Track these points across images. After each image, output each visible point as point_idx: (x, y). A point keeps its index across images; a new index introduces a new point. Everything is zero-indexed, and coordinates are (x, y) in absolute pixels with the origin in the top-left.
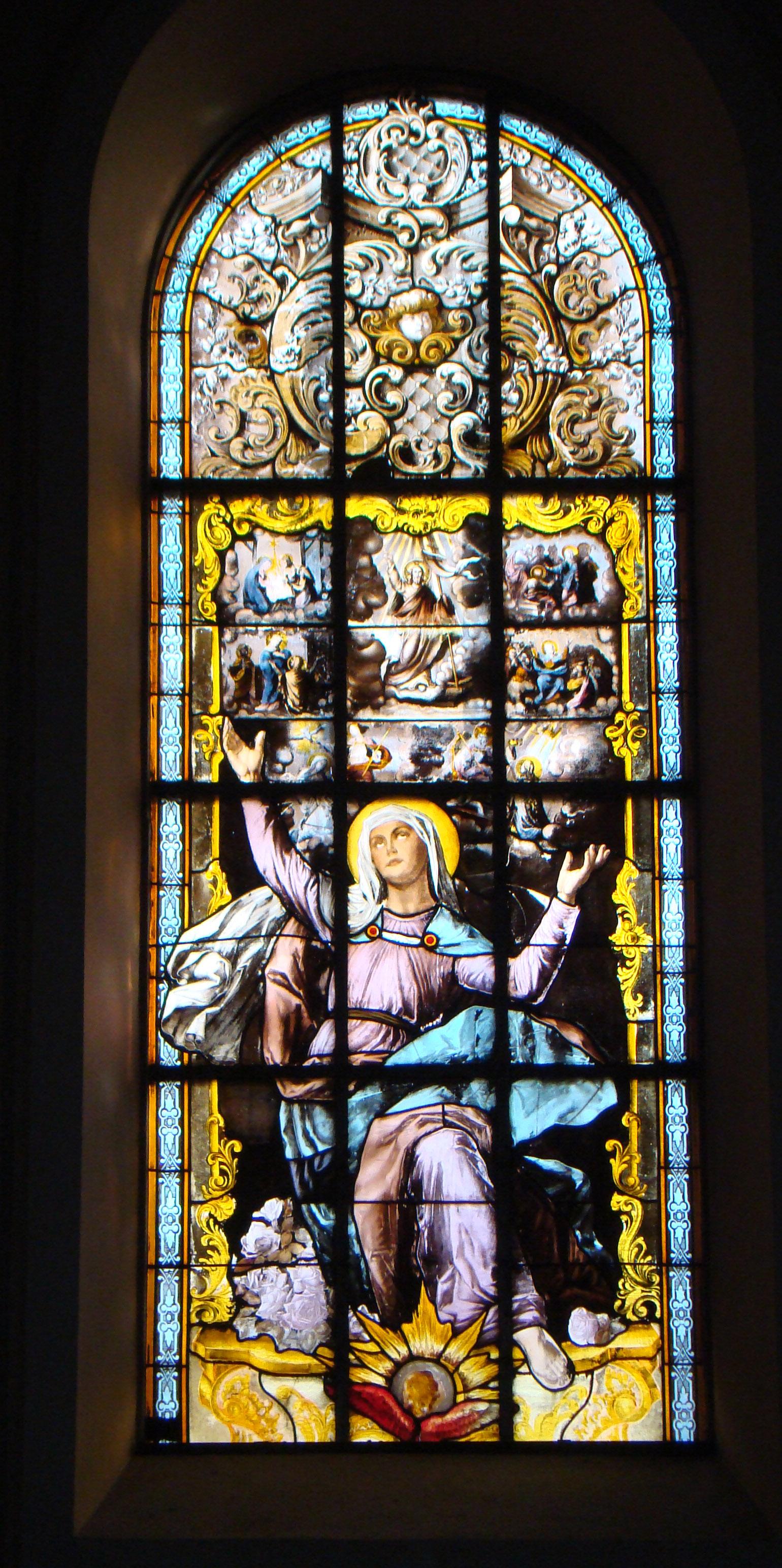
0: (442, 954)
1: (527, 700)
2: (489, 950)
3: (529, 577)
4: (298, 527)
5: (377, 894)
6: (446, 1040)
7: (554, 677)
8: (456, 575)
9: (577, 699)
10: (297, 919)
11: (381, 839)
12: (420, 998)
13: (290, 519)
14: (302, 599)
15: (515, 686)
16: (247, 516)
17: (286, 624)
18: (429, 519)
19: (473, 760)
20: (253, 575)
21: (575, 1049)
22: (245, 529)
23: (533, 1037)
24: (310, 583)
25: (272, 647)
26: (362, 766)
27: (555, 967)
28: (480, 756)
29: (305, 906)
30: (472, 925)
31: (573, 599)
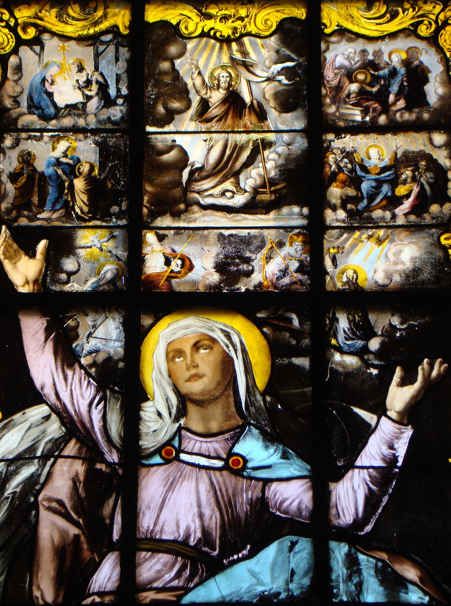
0: (250, 478)
1: (349, 206)
2: (305, 473)
3: (351, 82)
4: (91, 31)
5: (174, 411)
6: (253, 574)
7: (380, 183)
8: (269, 79)
9: (407, 205)
10: (78, 440)
11: (180, 353)
12: (223, 526)
13: (81, 24)
14: (93, 104)
15: (335, 192)
16: (32, 21)
17: (75, 130)
18: (238, 24)
19: (287, 268)
20: (38, 80)
21: (411, 587)
22: (32, 33)
23: (359, 572)
24: (103, 88)
25: (58, 153)
26: (159, 275)
27: (385, 493)
28: (294, 265)
29: (88, 425)
30: (285, 445)
31: (401, 104)
